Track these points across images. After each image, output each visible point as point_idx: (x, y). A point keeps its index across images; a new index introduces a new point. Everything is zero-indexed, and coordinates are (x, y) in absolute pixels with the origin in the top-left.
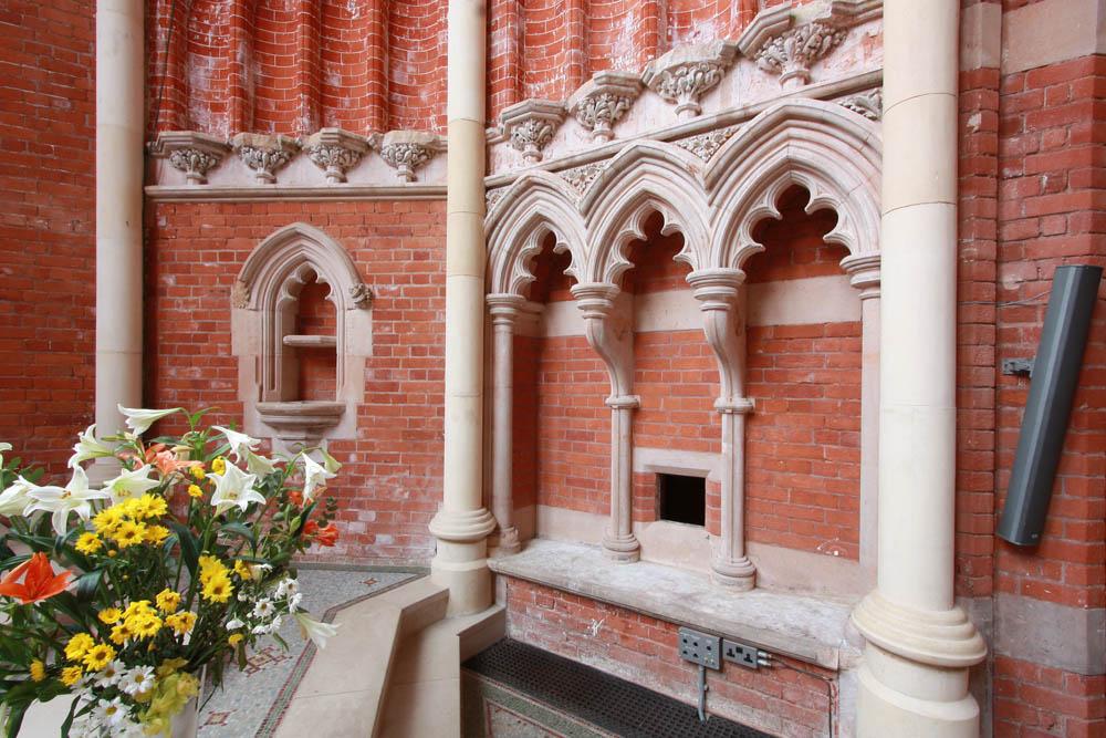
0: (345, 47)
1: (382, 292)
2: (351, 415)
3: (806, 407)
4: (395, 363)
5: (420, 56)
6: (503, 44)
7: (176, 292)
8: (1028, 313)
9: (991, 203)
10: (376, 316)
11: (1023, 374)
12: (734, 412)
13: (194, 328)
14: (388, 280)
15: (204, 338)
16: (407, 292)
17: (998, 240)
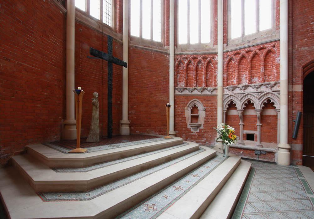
0: (199, 73)
1: (207, 108)
2: (202, 125)
3: (269, 125)
4: (209, 118)
5: (210, 75)
6: (225, 76)
7: (177, 108)
8: (295, 115)
9: (291, 104)
10: (206, 112)
11: (295, 122)
12: (260, 125)
13: (180, 113)
14: (207, 107)
15: (181, 114)
16: (210, 109)
17: (292, 108)
